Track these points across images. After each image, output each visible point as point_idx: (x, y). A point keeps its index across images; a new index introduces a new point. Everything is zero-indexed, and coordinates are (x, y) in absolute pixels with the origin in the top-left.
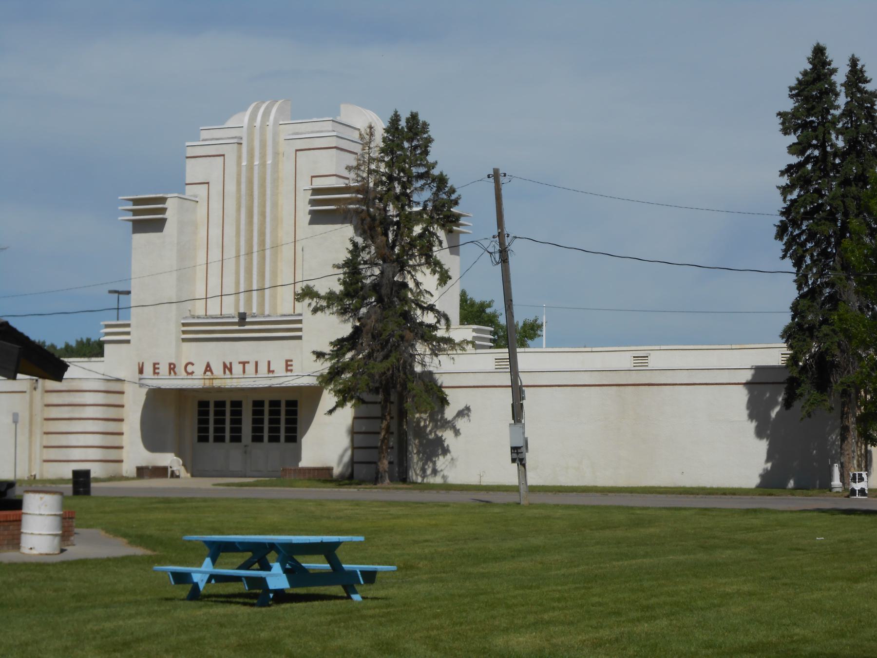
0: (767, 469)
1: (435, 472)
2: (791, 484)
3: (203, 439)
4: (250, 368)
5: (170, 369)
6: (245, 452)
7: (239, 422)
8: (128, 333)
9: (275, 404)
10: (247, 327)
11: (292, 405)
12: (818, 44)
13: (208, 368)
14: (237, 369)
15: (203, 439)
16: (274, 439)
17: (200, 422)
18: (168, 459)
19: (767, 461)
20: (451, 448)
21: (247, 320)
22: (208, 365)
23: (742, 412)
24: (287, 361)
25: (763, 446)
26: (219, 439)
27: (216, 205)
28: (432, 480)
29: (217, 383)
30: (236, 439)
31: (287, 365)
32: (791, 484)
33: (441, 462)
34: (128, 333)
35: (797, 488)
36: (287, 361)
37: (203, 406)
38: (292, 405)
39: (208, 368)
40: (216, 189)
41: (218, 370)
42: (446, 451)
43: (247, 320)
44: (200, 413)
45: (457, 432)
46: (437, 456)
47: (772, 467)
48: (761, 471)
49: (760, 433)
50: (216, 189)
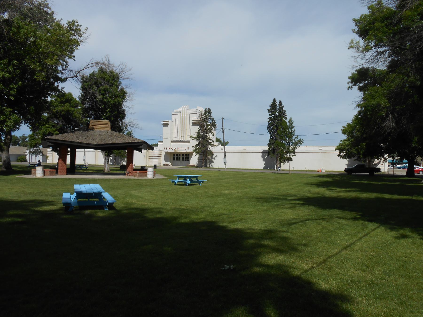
1: (211, 166)
2: (268, 168)
3: (174, 160)
4: (182, 149)
7: (180, 157)
11: (189, 155)
13: (175, 148)
14: (180, 149)
15: (174, 160)
18: (169, 163)
26: (177, 160)
29: (176, 151)
32: (268, 168)
33: (212, 164)
37: (174, 154)
38: (189, 155)
39: (175, 148)
41: (177, 149)
42: (213, 162)
45: (215, 159)
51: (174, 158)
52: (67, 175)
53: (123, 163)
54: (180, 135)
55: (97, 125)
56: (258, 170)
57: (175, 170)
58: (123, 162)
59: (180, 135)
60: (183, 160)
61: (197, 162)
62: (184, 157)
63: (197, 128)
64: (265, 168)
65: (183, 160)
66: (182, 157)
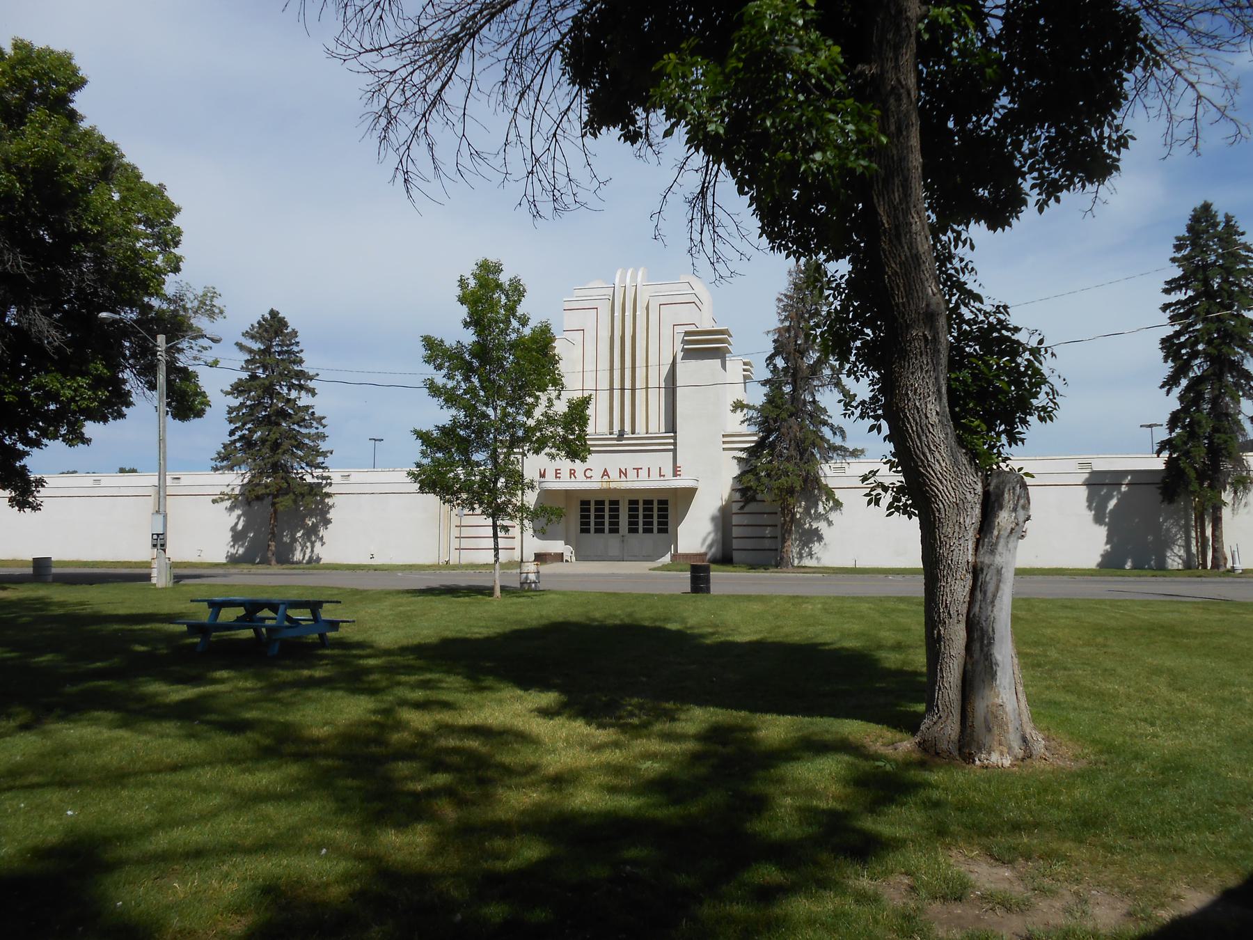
0: (1107, 551)
1: (811, 555)
2: (1128, 565)
3: (585, 530)
4: (643, 474)
5: (571, 474)
6: (623, 541)
7: (617, 517)
8: (724, 442)
9: (648, 503)
10: (624, 442)
11: (663, 504)
12: (1211, 204)
13: (605, 473)
14: (632, 475)
15: (585, 530)
16: (648, 531)
17: (582, 517)
18: (557, 546)
19: (1107, 543)
20: (824, 536)
21: (625, 436)
22: (605, 470)
23: (1084, 503)
24: (556, 470)
25: (1102, 531)
26: (599, 531)
27: (590, 348)
28: (807, 562)
29: (613, 485)
30: (614, 530)
31: (556, 473)
32: (1128, 565)
33: (816, 547)
34: (724, 442)
35: (1134, 567)
36: (556, 470)
37: (585, 505)
38: (663, 504)
39: (605, 473)
40: (590, 335)
41: (614, 475)
42: (820, 538)
43: (625, 436)
44: (582, 510)
45: (830, 523)
46: (813, 542)
47: (1111, 548)
48: (1102, 552)
49: (1098, 519)
50: (590, 335)
51: (582, 524)
52: (1013, 599)
53: (309, 550)
54: (611, 427)
55: (629, 313)
56: (1084, 575)
57: (281, 586)
58: (308, 544)
59: (611, 427)
60: (633, 530)
61: (709, 533)
62: (588, 517)
63: (766, 389)
64: (1110, 563)
65: (636, 531)
66: (630, 516)
